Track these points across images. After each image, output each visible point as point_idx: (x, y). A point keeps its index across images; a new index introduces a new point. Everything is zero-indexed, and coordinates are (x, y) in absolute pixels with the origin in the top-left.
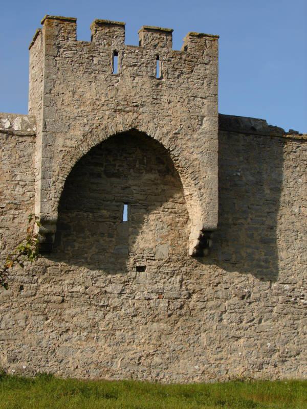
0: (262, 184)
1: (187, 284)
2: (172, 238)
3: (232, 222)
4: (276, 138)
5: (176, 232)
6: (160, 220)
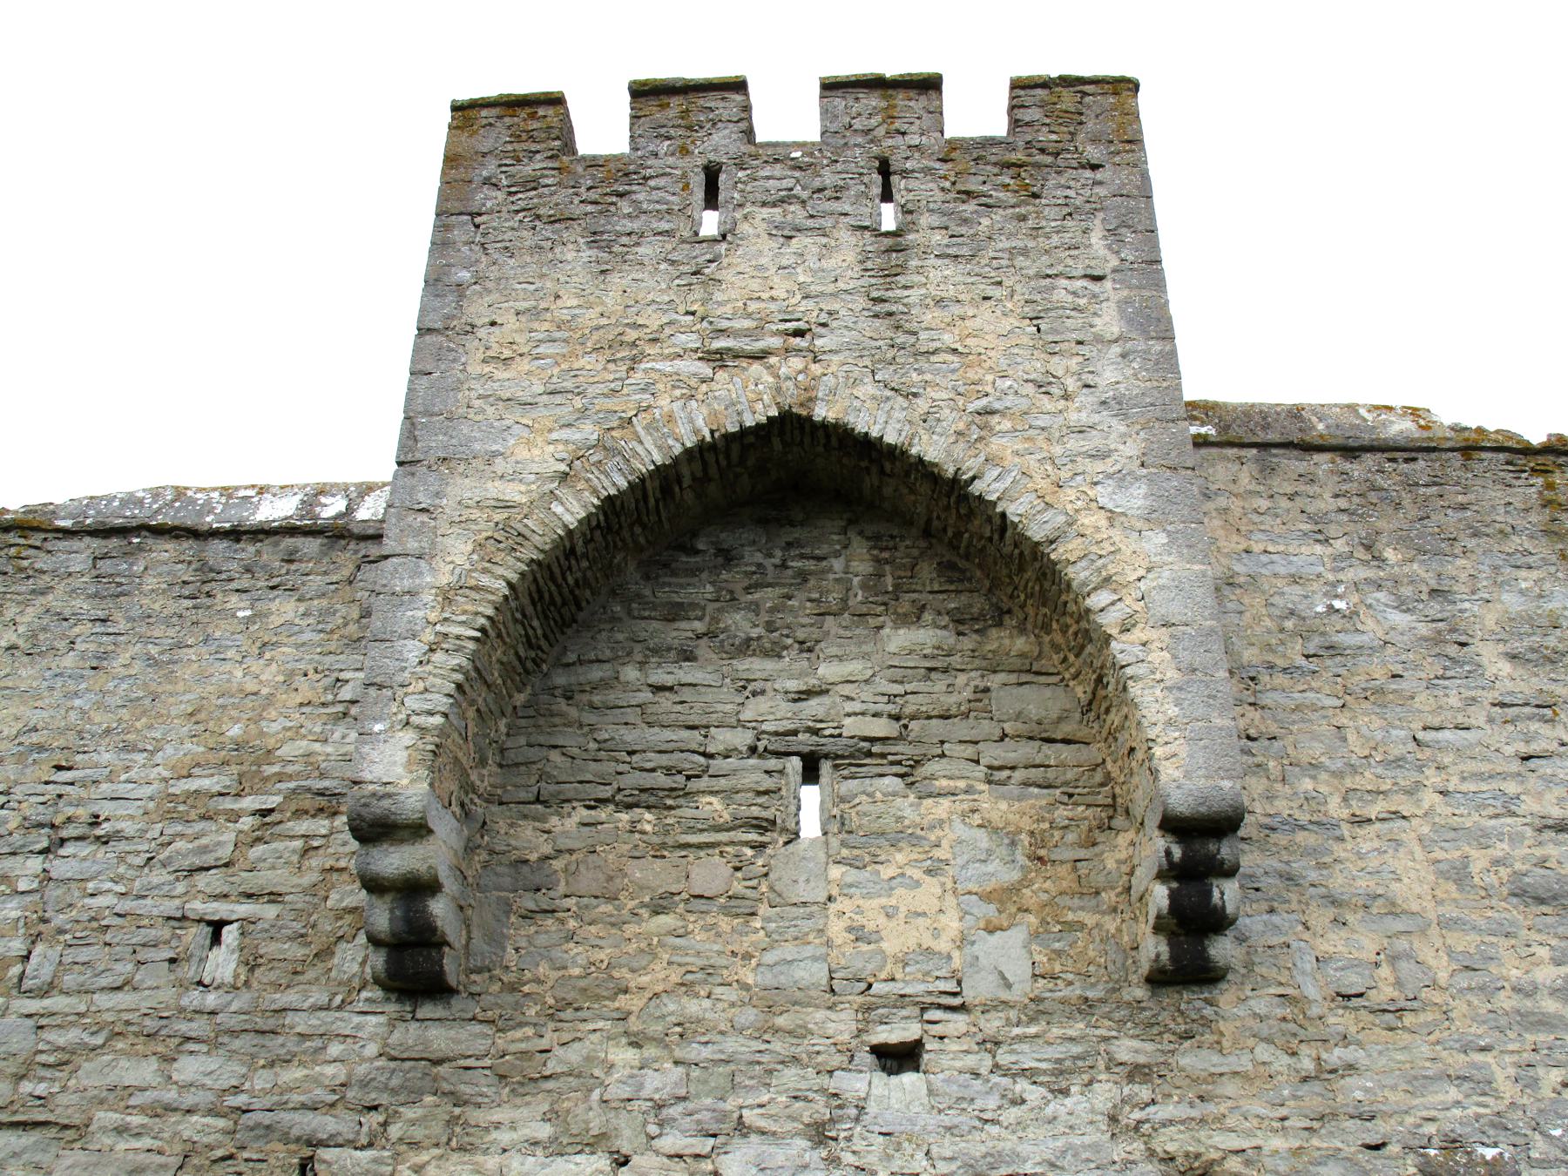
0: (1463, 639)
1: (1146, 1127)
2: (1045, 897)
3: (1345, 813)
4: (1484, 455)
5: (1063, 870)
6: (976, 819)
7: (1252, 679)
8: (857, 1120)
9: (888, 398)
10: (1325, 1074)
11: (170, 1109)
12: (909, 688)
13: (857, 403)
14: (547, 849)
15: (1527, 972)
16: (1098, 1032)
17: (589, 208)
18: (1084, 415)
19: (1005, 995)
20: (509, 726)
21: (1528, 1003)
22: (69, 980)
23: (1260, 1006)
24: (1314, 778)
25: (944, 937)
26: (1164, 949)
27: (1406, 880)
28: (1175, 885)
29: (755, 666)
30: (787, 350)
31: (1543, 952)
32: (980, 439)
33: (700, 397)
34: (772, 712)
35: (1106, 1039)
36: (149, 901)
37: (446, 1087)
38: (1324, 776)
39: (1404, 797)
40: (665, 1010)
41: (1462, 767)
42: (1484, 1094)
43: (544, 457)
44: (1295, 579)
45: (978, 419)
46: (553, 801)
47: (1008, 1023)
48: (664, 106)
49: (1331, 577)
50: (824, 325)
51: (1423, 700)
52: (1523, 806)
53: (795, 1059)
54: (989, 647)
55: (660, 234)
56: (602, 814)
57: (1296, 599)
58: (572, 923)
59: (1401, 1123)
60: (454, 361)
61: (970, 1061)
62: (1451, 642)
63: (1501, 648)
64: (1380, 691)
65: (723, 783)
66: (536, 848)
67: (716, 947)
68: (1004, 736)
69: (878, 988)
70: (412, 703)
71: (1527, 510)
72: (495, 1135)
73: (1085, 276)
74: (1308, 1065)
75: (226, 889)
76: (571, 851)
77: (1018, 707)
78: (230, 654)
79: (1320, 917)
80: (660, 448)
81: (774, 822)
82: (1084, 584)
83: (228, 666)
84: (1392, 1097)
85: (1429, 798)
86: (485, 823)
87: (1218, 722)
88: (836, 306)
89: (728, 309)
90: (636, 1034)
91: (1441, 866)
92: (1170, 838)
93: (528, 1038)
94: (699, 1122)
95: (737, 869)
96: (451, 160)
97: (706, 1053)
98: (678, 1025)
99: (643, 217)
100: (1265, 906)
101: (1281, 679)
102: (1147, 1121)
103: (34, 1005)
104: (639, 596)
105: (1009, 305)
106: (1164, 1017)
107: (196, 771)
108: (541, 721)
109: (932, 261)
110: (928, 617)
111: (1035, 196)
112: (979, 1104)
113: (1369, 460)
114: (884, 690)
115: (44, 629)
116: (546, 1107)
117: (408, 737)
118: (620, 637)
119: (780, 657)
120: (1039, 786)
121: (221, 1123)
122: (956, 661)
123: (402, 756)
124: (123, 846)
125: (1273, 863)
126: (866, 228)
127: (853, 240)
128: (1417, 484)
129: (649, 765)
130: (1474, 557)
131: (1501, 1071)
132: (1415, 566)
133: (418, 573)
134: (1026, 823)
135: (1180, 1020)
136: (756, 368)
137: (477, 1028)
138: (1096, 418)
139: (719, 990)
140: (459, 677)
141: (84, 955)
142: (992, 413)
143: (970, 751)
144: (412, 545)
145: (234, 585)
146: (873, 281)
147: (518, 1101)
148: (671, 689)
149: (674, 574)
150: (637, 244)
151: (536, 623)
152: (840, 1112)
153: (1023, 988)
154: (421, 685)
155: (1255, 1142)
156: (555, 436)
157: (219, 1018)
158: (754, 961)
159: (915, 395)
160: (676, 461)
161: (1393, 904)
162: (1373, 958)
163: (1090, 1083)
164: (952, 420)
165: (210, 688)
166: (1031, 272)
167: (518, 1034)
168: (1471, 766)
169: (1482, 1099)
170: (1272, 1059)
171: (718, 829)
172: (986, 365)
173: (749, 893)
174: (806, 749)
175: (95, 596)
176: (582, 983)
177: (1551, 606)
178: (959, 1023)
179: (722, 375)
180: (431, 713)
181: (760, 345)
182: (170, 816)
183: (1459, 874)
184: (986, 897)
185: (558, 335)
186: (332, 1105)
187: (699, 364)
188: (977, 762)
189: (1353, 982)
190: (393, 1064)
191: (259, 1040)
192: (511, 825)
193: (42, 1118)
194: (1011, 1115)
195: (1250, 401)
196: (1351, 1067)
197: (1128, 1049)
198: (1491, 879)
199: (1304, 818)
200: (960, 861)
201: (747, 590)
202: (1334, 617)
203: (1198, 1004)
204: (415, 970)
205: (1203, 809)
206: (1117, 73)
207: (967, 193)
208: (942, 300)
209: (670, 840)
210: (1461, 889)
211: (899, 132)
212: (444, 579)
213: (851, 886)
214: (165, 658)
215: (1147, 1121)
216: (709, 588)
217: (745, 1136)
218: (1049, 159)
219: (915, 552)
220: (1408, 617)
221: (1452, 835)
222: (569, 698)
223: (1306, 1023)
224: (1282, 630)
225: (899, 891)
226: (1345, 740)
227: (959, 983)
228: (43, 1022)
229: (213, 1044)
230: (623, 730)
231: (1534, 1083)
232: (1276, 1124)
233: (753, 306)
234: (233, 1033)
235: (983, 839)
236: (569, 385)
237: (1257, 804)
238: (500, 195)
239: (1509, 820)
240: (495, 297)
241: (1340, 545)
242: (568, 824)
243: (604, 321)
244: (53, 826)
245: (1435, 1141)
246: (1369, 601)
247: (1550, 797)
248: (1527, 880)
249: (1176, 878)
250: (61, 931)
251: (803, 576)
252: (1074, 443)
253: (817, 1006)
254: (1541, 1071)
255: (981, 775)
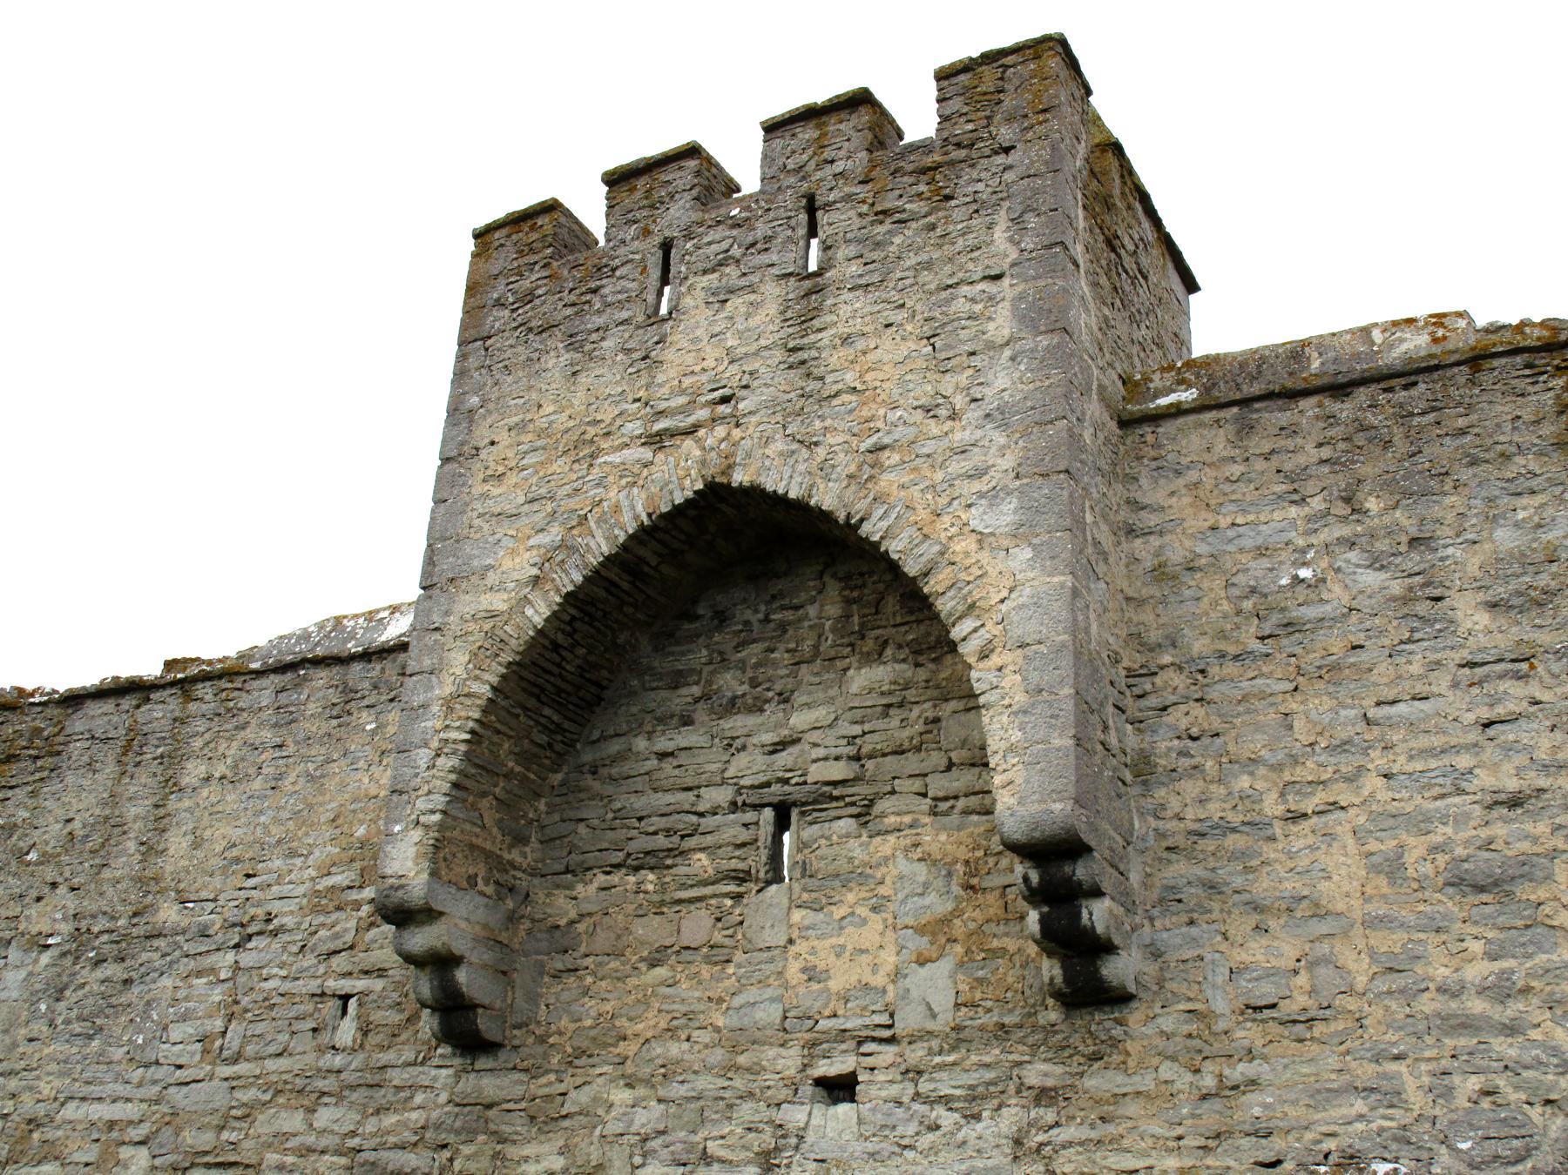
0: (1437, 592)
1: (1047, 1150)
2: (972, 925)
3: (1280, 810)
4: (1496, 363)
5: (991, 898)
6: (919, 853)
7: (1202, 671)
8: (797, 1148)
9: (793, 452)
10: (1230, 1090)
11: (311, 1150)
12: (867, 727)
13: (767, 463)
14: (573, 914)
15: (1457, 970)
16: (1011, 1057)
17: (569, 311)
18: (968, 432)
19: (930, 1025)
20: (547, 804)
21: (1454, 1005)
22: (250, 1050)
23: (1167, 1023)
24: (1251, 774)
25: (882, 973)
26: (1057, 972)
27: (1335, 878)
28: (1046, 909)
29: (738, 724)
30: (714, 420)
31: (1476, 947)
32: (871, 477)
33: (641, 482)
34: (750, 766)
35: (1019, 1064)
36: (301, 982)
37: (492, 1127)
38: (1262, 771)
39: (1344, 785)
40: (654, 1054)
41: (1413, 744)
42: (1392, 1106)
43: (521, 565)
44: (1261, 551)
45: (870, 458)
46: (579, 870)
47: (931, 1052)
48: (632, 190)
49: (1301, 542)
50: (746, 387)
51: (1384, 670)
52: (1475, 781)
53: (751, 1094)
54: (943, 675)
55: (621, 323)
56: (615, 879)
57: (1259, 573)
58: (589, 979)
59: (1298, 1140)
60: (464, 485)
61: (894, 1090)
62: (1427, 595)
63: (1481, 596)
64: (1335, 668)
65: (709, 840)
66: (566, 913)
67: (697, 994)
68: (950, 766)
69: (824, 1024)
70: (421, 804)
71: (1538, 422)
72: (524, 1167)
73: (985, 278)
74: (1209, 1082)
75: (349, 968)
76: (590, 914)
77: (963, 734)
78: (361, 764)
79: (1240, 925)
80: (607, 539)
81: (749, 872)
82: (951, 614)
83: (359, 775)
84: (1292, 1112)
85: (1372, 783)
86: (528, 895)
87: (1057, 742)
88: (757, 365)
89: (666, 390)
90: (630, 1076)
91: (1374, 859)
92: (1027, 865)
93: (551, 1083)
94: (673, 1153)
95: (719, 920)
96: (472, 289)
97: (683, 1091)
98: (663, 1066)
99: (609, 310)
100: (1184, 918)
101: (1231, 668)
102: (1049, 1143)
103: (228, 1071)
104: (651, 668)
105: (909, 328)
106: (1075, 1040)
107: (333, 870)
108: (571, 798)
109: (846, 296)
110: (889, 652)
111: (948, 198)
112: (900, 1130)
113: (1362, 395)
114: (845, 733)
115: (243, 759)
116: (561, 1143)
117: (416, 835)
118: (634, 710)
119: (762, 710)
120: (979, 813)
121: (343, 1161)
122: (911, 695)
123: (412, 851)
124: (286, 937)
125: (1199, 871)
126: (791, 274)
127: (777, 291)
128: (1412, 414)
129: (651, 829)
130: (1466, 491)
131: (1412, 1081)
132: (1398, 513)
133: (430, 688)
134: (963, 853)
135: (1089, 1041)
136: (688, 443)
137: (517, 1076)
138: (979, 433)
139: (696, 1033)
140: (453, 777)
141: (259, 1028)
142: (883, 448)
143: (917, 785)
144: (427, 663)
145: (366, 702)
146: (791, 330)
147: (543, 1138)
148: (672, 754)
149: (678, 643)
150: (603, 339)
151: (547, 711)
152: (783, 1141)
153: (942, 1023)
154: (426, 788)
155: (1148, 1162)
156: (532, 542)
157: (343, 1076)
158: (724, 1006)
159: (816, 444)
160: (624, 547)
161: (1317, 905)
162: (1292, 964)
163: (999, 1107)
164: (845, 464)
165: (347, 796)
166: (933, 287)
167: (543, 1080)
168: (1423, 742)
169: (1390, 1111)
170: (1175, 1077)
171: (705, 883)
172: (879, 400)
173: (727, 942)
174: (776, 800)
175: (276, 725)
176: (593, 1033)
177: (1550, 536)
178: (888, 1054)
179: (661, 456)
180: (433, 812)
181: (691, 420)
182: (316, 910)
183: (1393, 867)
184: (920, 930)
185: (539, 443)
186: (415, 1144)
187: (642, 449)
188: (925, 795)
189: (1265, 992)
190: (457, 1109)
191: (369, 1092)
192: (547, 895)
193: (232, 1159)
194: (928, 1139)
195: (1254, 346)
196: (1253, 1082)
197: (1038, 1073)
198: (1428, 868)
199: (1235, 819)
200: (900, 896)
201: (737, 648)
202: (1300, 588)
203: (1108, 1024)
204: (463, 1031)
205: (1037, 834)
206: (1037, 34)
207: (884, 212)
208: (849, 336)
209: (667, 898)
210: (1392, 881)
211: (827, 162)
212: (448, 689)
213: (808, 928)
214: (318, 773)
215: (1049, 1143)
216: (705, 652)
217: (708, 1164)
218: (963, 153)
219: (881, 586)
220: (1383, 575)
221: (1391, 822)
222: (594, 773)
223: (1212, 1040)
224: (1239, 612)
225: (850, 929)
226: (1291, 727)
227: (892, 1016)
228: (234, 1083)
229: (340, 1098)
230: (633, 798)
231: (1448, 1093)
232: (1171, 1144)
233: (687, 382)
234: (353, 1088)
235: (922, 872)
236: (543, 491)
237: (1189, 809)
238: (507, 313)
239: (1457, 800)
240: (495, 416)
241: (1317, 504)
242: (588, 890)
243: (571, 423)
244: (243, 925)
245: (1333, 1159)
246: (1339, 564)
247: (1508, 767)
248: (1466, 865)
249: (1046, 901)
250: (246, 1011)
251: (783, 627)
252: (956, 466)
253: (771, 1044)
254: (1456, 1079)
255: (925, 808)
